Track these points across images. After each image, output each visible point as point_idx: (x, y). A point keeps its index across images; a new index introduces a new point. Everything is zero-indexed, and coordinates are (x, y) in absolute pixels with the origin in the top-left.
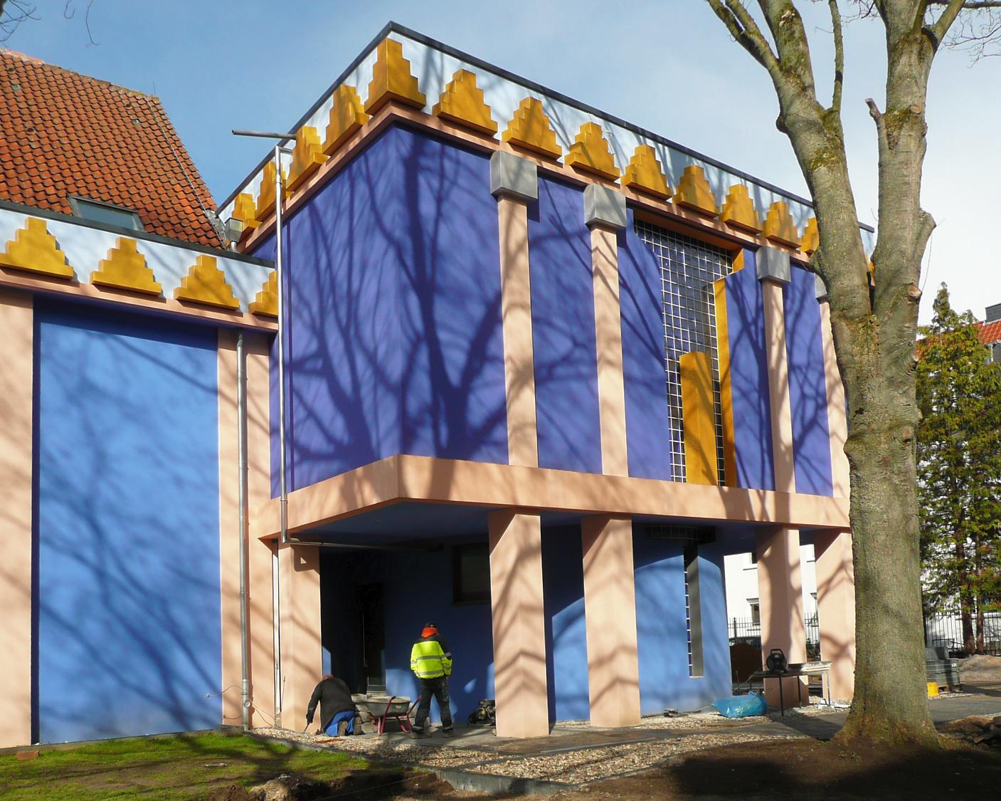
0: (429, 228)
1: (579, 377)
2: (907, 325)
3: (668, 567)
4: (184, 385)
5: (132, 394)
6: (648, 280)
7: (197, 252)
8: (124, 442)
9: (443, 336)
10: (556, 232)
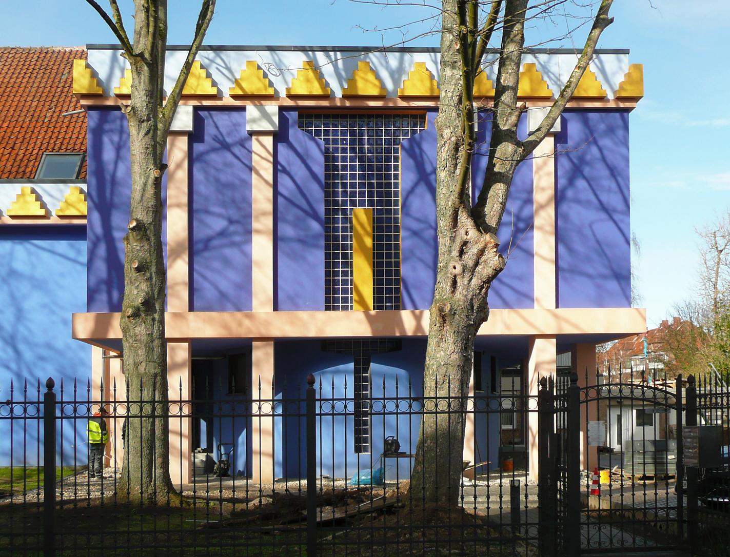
0: (110, 167)
1: (233, 244)
2: (135, 244)
4: (69, 264)
5: (39, 273)
6: (309, 162)
8: (33, 302)
10: (217, 145)
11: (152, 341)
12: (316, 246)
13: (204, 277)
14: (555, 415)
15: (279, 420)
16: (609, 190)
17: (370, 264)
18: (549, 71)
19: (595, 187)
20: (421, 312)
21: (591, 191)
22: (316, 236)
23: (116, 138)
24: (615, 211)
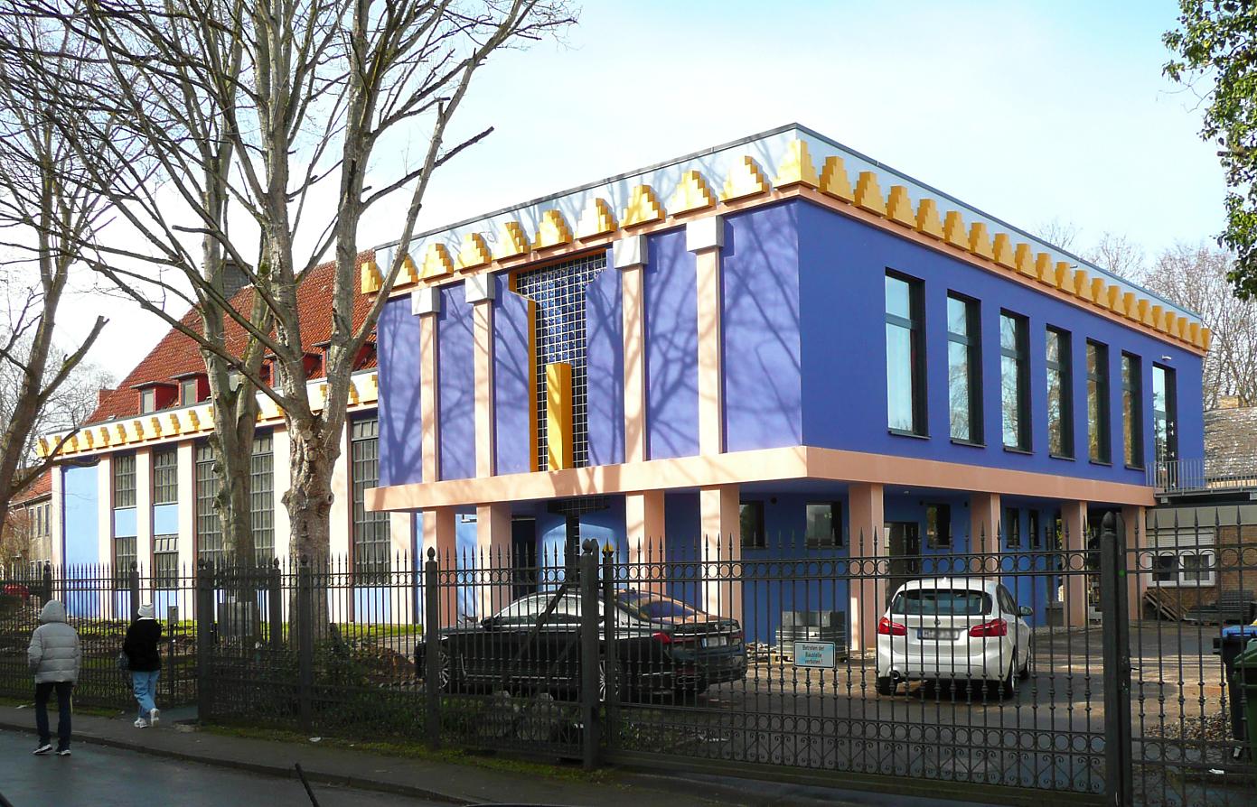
3: (555, 534)
6: (516, 323)
7: (527, 367)
9: (394, 415)
11: (229, 526)
12: (521, 408)
13: (447, 448)
14: (215, 591)
15: (737, 585)
16: (775, 304)
17: (558, 421)
18: (714, 173)
19: (761, 303)
20: (594, 469)
21: (757, 309)
22: (521, 398)
23: (392, 328)
24: (781, 328)
